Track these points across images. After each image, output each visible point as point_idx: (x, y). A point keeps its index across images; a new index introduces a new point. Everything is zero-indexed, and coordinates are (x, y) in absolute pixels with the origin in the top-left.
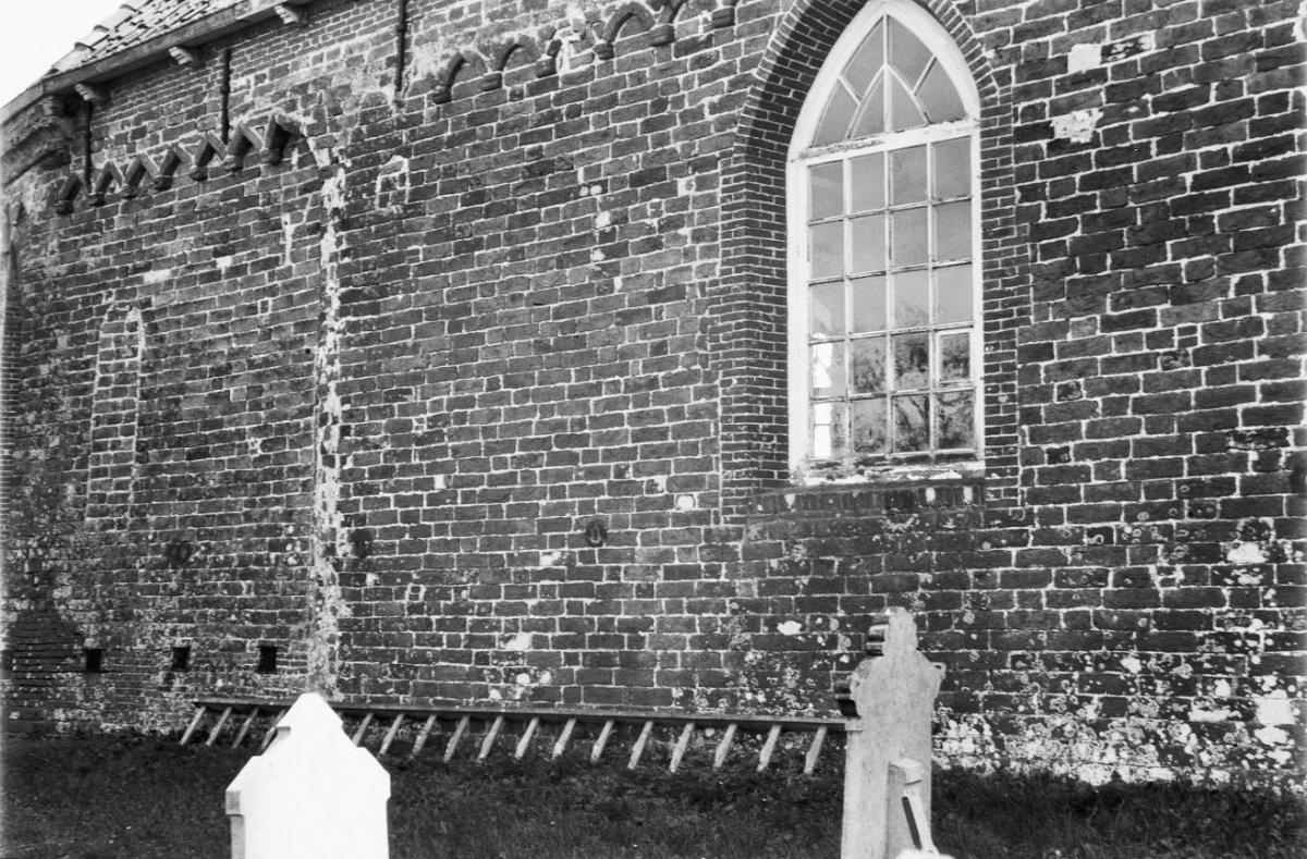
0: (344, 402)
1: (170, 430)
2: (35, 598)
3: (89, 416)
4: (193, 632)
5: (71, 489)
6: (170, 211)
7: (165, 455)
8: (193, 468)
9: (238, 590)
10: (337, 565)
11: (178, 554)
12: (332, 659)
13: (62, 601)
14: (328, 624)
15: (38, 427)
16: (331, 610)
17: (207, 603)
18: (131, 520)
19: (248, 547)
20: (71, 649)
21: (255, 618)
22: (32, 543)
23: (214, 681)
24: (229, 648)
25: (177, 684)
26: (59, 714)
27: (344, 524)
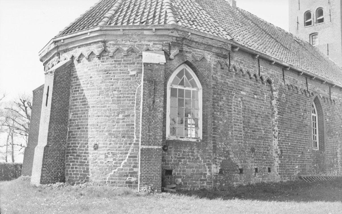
0: (278, 129)
1: (249, 125)
2: (226, 157)
3: (232, 117)
4: (258, 165)
5: (230, 133)
6: (245, 81)
7: (249, 130)
8: (254, 134)
9: (263, 158)
10: (278, 155)
11: (253, 150)
12: (278, 170)
13: (232, 158)
14: (276, 164)
15: (220, 116)
16: (277, 162)
17: (259, 160)
18: (243, 142)
19: (264, 150)
20: (236, 169)
21: (266, 163)
22: (223, 144)
23: (262, 174)
24: (264, 168)
25: (257, 175)
26: (235, 183)
27: (279, 148)
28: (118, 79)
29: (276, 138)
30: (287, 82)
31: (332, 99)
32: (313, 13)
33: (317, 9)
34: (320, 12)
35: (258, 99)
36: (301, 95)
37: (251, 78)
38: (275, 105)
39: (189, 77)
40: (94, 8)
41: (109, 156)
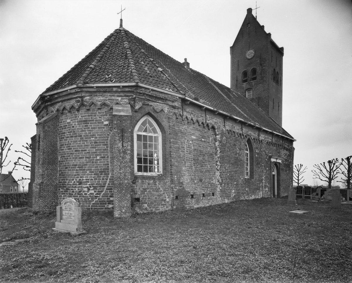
29: (219, 171)
30: (228, 128)
33: (252, 69)
34: (254, 71)
35: (205, 142)
36: (237, 137)
39: (151, 125)
41: (91, 189)
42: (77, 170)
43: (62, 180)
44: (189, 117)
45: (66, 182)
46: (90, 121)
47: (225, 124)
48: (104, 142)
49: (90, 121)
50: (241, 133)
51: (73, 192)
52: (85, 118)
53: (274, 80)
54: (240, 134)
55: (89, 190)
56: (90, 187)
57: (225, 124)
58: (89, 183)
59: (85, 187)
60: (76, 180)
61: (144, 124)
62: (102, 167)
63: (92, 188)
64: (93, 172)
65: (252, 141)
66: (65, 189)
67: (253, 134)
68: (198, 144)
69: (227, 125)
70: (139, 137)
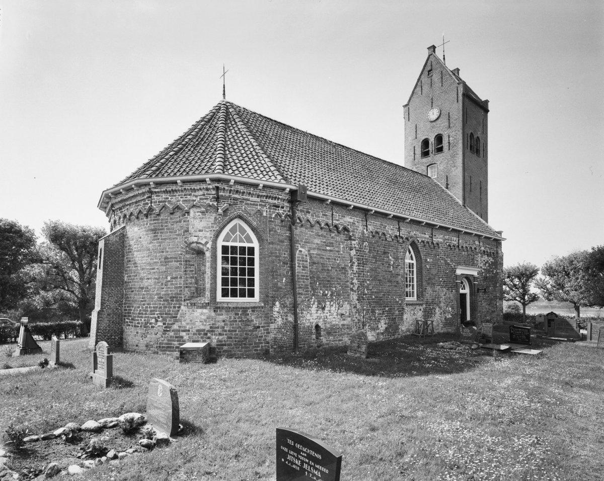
28: (165, 239)
29: (355, 292)
30: (370, 228)
31: (435, 243)
32: (432, 140)
33: (436, 136)
34: (439, 138)
35: (330, 251)
36: (390, 241)
37: (322, 228)
38: (354, 255)
39: (243, 231)
40: (157, 157)
41: (159, 320)
42: (144, 294)
43: (128, 307)
44: (303, 218)
45: (132, 310)
46: (161, 229)
47: (366, 224)
48: (176, 258)
49: (161, 229)
50: (398, 234)
51: (138, 323)
52: (154, 226)
53: (471, 149)
54: (396, 236)
55: (157, 321)
56: (158, 317)
57: (366, 224)
58: (158, 312)
59: (152, 318)
60: (142, 308)
61: (233, 230)
62: (174, 291)
63: (161, 319)
64: (162, 298)
65: (420, 246)
66: (130, 318)
67: (423, 236)
68: (319, 255)
69: (370, 225)
70: (225, 249)
